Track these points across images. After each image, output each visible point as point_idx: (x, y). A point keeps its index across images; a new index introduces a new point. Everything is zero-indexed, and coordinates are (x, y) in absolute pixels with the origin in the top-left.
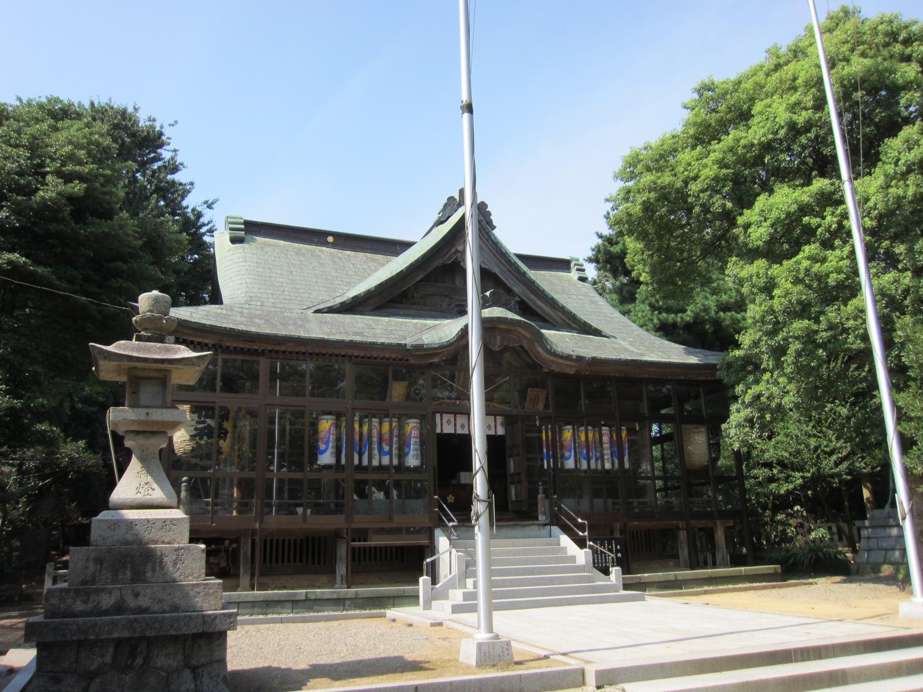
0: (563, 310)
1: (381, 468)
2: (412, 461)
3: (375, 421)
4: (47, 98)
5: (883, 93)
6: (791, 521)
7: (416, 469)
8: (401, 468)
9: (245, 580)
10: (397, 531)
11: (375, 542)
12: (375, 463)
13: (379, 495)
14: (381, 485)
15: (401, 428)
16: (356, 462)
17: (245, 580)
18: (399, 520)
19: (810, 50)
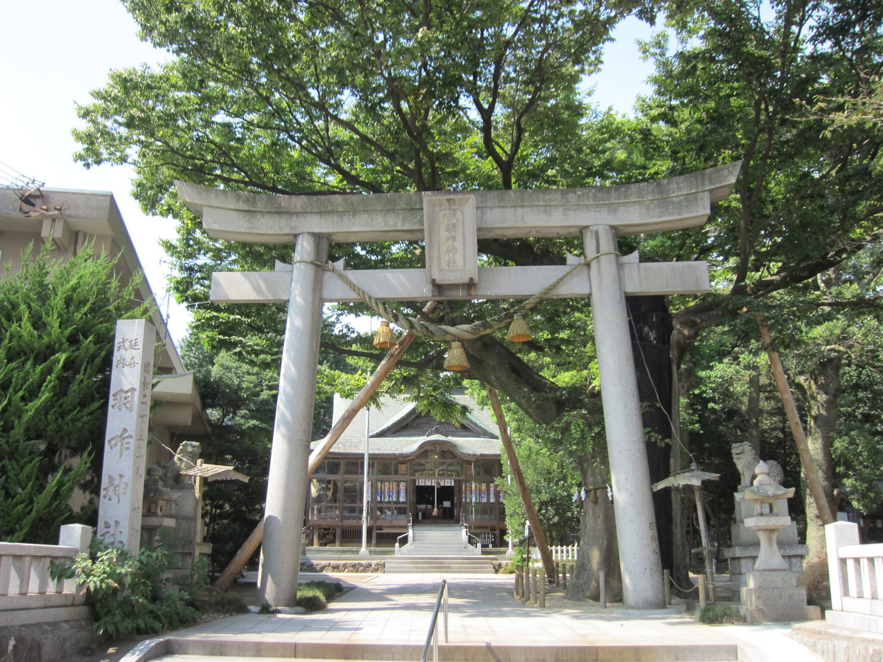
0: (484, 429)
1: (389, 502)
2: (402, 499)
3: (387, 483)
4: (84, 492)
5: (276, 67)
6: (827, 309)
7: (403, 503)
8: (398, 502)
9: (338, 543)
10: (394, 527)
11: (385, 531)
12: (387, 500)
13: (389, 513)
14: (389, 509)
15: (398, 486)
16: (379, 499)
17: (338, 543)
18: (395, 523)
19: (156, 370)
